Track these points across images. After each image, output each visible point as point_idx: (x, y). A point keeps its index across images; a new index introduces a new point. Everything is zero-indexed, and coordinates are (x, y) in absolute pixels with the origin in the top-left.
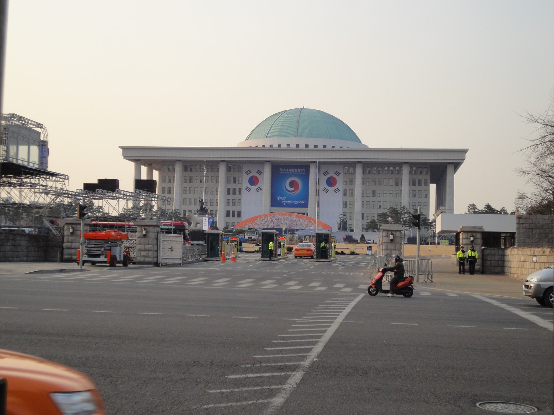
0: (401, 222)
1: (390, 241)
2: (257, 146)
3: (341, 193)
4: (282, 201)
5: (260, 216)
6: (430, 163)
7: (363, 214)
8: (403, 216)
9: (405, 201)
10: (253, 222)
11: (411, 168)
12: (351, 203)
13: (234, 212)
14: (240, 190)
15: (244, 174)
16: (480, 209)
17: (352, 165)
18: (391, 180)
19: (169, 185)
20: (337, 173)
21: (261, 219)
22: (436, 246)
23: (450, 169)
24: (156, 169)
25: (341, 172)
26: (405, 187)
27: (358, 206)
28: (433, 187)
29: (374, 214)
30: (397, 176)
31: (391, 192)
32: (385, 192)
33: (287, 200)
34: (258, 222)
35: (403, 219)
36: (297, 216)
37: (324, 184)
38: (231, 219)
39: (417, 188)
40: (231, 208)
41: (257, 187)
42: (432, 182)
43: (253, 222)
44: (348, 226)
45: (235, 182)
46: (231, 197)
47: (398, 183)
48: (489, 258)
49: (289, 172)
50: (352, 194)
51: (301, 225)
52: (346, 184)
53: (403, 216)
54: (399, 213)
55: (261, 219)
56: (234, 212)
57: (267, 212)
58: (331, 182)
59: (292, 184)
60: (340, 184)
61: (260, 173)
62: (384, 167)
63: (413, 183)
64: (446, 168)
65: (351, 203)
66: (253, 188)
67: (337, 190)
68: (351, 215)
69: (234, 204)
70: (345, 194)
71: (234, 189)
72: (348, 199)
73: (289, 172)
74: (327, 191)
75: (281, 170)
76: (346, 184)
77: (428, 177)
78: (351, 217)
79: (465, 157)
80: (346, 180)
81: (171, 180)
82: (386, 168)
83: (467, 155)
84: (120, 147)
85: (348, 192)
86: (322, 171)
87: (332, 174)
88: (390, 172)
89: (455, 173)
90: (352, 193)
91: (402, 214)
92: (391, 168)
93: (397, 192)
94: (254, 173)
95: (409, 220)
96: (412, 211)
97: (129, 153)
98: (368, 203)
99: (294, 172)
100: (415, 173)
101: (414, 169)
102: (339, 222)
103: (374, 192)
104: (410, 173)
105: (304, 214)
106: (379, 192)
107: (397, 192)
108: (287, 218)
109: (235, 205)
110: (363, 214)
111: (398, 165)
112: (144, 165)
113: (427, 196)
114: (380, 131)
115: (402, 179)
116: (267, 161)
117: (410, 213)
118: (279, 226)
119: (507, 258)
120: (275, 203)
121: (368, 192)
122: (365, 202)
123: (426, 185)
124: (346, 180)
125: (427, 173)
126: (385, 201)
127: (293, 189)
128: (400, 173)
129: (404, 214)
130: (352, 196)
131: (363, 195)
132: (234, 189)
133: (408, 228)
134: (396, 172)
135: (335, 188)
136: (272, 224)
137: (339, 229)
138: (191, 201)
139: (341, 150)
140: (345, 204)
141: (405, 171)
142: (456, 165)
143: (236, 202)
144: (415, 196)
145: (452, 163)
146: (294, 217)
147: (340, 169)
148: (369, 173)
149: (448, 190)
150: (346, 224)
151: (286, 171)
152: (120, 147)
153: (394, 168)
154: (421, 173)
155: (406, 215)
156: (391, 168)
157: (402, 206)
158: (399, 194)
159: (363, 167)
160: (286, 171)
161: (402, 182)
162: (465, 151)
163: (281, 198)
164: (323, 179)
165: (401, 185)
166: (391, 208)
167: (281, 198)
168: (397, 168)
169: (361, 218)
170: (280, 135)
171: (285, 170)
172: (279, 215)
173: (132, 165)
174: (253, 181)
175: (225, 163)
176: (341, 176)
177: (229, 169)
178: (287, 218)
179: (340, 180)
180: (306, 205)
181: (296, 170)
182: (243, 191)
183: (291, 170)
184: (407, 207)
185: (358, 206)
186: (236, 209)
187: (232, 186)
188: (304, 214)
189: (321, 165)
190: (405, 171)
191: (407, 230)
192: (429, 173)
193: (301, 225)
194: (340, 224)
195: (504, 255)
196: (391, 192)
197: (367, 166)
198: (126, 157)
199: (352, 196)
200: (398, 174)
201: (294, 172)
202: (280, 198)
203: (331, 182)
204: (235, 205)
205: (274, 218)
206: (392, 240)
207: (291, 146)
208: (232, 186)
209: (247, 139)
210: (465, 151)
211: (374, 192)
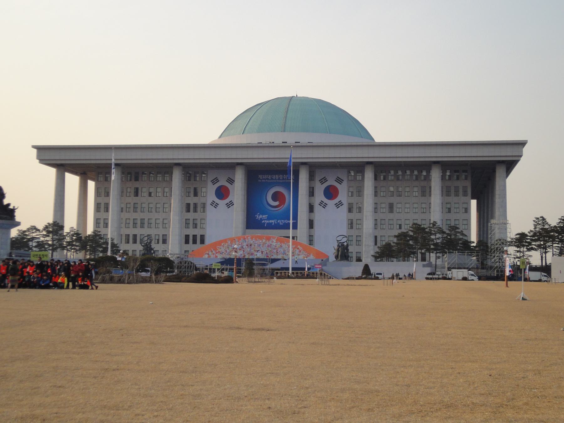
0: (430, 245)
3: (345, 208)
4: (261, 219)
5: (225, 241)
7: (376, 237)
8: (433, 237)
9: (436, 215)
10: (215, 250)
11: (444, 172)
12: (359, 222)
13: (195, 237)
14: (204, 206)
15: (210, 184)
16: (553, 225)
17: (358, 168)
18: (416, 189)
19: (105, 200)
20: (339, 181)
21: (226, 245)
22: (504, 283)
23: (500, 171)
24: (92, 179)
25: (344, 176)
26: (436, 198)
27: (368, 225)
28: (474, 203)
29: (390, 236)
30: (423, 184)
31: (416, 206)
32: (407, 206)
33: (268, 219)
34: (222, 250)
35: (433, 240)
37: (319, 196)
38: (191, 247)
40: (191, 232)
41: (227, 201)
43: (215, 250)
45: (196, 194)
46: (191, 215)
47: (426, 192)
49: (272, 179)
50: (360, 210)
53: (433, 237)
54: (426, 233)
55: (226, 245)
56: (195, 237)
57: (240, 234)
58: (331, 193)
60: (343, 196)
61: (231, 181)
62: (403, 169)
64: (494, 171)
65: (359, 222)
66: (222, 203)
68: (359, 239)
69: (195, 226)
70: (350, 210)
71: (195, 205)
72: (354, 216)
73: (272, 179)
74: (325, 206)
75: (260, 176)
78: (359, 242)
79: (522, 151)
80: (351, 189)
81: (107, 194)
82: (408, 172)
83: (525, 149)
84: (34, 147)
85: (355, 207)
86: (318, 178)
87: (331, 182)
88: (414, 177)
89: (507, 176)
90: (360, 208)
91: (431, 234)
92: (416, 173)
93: (424, 206)
94: (223, 182)
95: (442, 243)
97: (49, 155)
98: (383, 222)
99: (279, 179)
102: (336, 247)
103: (391, 207)
104: (443, 178)
106: (399, 206)
107: (424, 206)
108: (264, 244)
109: (196, 227)
110: (376, 237)
111: (425, 166)
113: (467, 210)
114: (395, 119)
115: (430, 187)
117: (444, 233)
118: (252, 254)
120: (252, 223)
121: (383, 206)
122: (379, 221)
124: (351, 189)
125: (466, 179)
126: (406, 217)
127: (277, 203)
128: (428, 178)
129: (435, 234)
130: (360, 212)
131: (376, 210)
132: (195, 205)
133: (440, 255)
134: (422, 178)
135: (336, 201)
136: (242, 252)
137: (337, 257)
140: (351, 225)
141: (369, 175)
142: (510, 165)
143: (198, 222)
147: (342, 174)
148: (384, 179)
149: (497, 200)
151: (268, 179)
152: (34, 147)
153: (420, 172)
154: (458, 178)
155: (438, 235)
157: (432, 222)
160: (268, 179)
161: (430, 191)
162: (523, 144)
163: (261, 216)
164: (320, 189)
165: (430, 196)
166: (414, 224)
167: (261, 216)
169: (373, 243)
171: (266, 177)
172: (252, 238)
173: (53, 171)
174: (222, 193)
175: (181, 167)
176: (345, 183)
178: (264, 244)
179: (343, 189)
181: (281, 176)
182: (209, 207)
183: (274, 177)
184: (439, 223)
185: (368, 225)
186: (198, 232)
187: (192, 200)
189: (314, 168)
190: (369, 175)
191: (439, 257)
192: (469, 178)
194: (338, 250)
196: (416, 206)
197: (383, 169)
198: (43, 161)
199: (360, 212)
200: (425, 180)
201: (279, 179)
202: (259, 217)
203: (331, 193)
204: (196, 227)
205: (245, 244)
208: (192, 200)
209: (220, 137)
210: (523, 144)
211: (391, 207)
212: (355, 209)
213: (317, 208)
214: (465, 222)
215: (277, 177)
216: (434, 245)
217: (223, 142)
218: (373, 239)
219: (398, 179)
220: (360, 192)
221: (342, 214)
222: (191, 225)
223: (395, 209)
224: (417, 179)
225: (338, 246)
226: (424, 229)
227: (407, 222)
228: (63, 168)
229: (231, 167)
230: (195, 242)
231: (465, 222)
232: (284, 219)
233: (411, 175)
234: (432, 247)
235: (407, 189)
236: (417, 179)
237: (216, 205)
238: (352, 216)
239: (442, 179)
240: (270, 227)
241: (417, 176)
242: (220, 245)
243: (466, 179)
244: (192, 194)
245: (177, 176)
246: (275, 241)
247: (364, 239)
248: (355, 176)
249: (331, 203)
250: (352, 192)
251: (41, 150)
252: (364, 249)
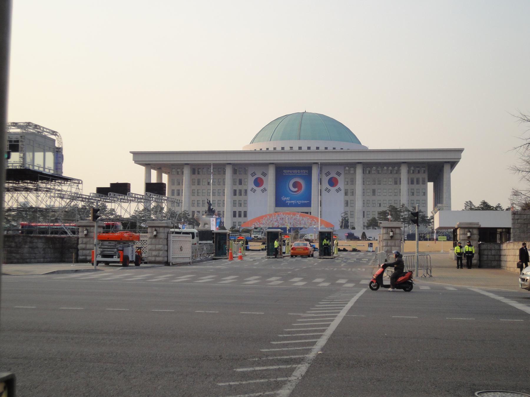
1: (390, 238)
2: (261, 149)
3: (343, 192)
5: (266, 216)
6: (428, 163)
7: (364, 212)
8: (402, 214)
10: (259, 222)
16: (477, 206)
17: (353, 165)
18: (390, 180)
19: (178, 187)
20: (339, 174)
21: (266, 219)
23: (446, 168)
24: (165, 173)
25: (341, 171)
26: (404, 186)
27: (359, 205)
29: (374, 212)
32: (385, 191)
33: (290, 200)
34: (264, 222)
35: (402, 216)
36: (300, 216)
37: (325, 185)
38: (237, 219)
39: (415, 186)
40: (237, 209)
41: (262, 188)
42: (429, 181)
43: (259, 222)
44: (349, 224)
45: (240, 183)
46: (237, 198)
47: (397, 182)
48: (486, 252)
50: (353, 193)
51: (305, 224)
52: (347, 184)
53: (402, 214)
55: (266, 219)
57: (272, 212)
58: (333, 182)
59: (295, 185)
60: (341, 184)
61: (264, 174)
63: (411, 182)
64: (443, 167)
67: (338, 190)
68: (352, 213)
69: (240, 205)
70: (346, 194)
73: (293, 173)
75: (285, 171)
76: (347, 184)
77: (426, 176)
78: (352, 215)
79: (461, 156)
80: (347, 180)
81: (180, 183)
82: (385, 168)
83: (463, 154)
84: (131, 152)
85: (349, 191)
86: (324, 171)
87: (333, 175)
88: (389, 171)
89: (451, 172)
90: (353, 192)
92: (390, 168)
93: (396, 191)
94: (259, 175)
95: (408, 218)
96: (411, 209)
98: (368, 202)
99: (298, 173)
100: (413, 173)
101: (412, 168)
102: (341, 220)
103: (374, 191)
104: (409, 172)
105: (307, 213)
106: (379, 191)
107: (396, 191)
109: (241, 206)
110: (364, 212)
112: (154, 169)
113: (425, 194)
114: (379, 132)
115: (400, 179)
116: (358, 163)
117: (409, 211)
118: (284, 225)
119: (503, 253)
120: (279, 203)
121: (368, 191)
123: (424, 183)
124: (347, 180)
125: (424, 172)
126: (384, 200)
127: (296, 189)
128: (398, 172)
130: (353, 195)
133: (407, 225)
134: (395, 172)
135: (337, 187)
137: (341, 227)
138: (199, 191)
139: (342, 151)
140: (347, 203)
141: (404, 170)
142: (453, 164)
144: (413, 195)
145: (448, 162)
146: (298, 217)
150: (348, 222)
151: (290, 173)
152: (131, 152)
153: (393, 167)
154: (419, 172)
155: (406, 213)
156: (390, 168)
158: (398, 193)
159: (363, 168)
160: (290, 173)
161: (400, 182)
162: (461, 151)
163: (285, 198)
164: (325, 180)
165: (400, 184)
167: (285, 198)
168: (396, 168)
169: (362, 216)
170: (282, 139)
171: (288, 171)
172: (283, 214)
173: (143, 168)
174: (258, 182)
175: (231, 166)
176: (342, 176)
177: (235, 172)
180: (309, 205)
181: (299, 171)
182: (249, 192)
183: (294, 171)
185: (359, 205)
186: (242, 209)
187: (238, 187)
188: (307, 213)
189: (322, 166)
190: (404, 170)
191: (406, 227)
192: (427, 173)
193: (305, 224)
194: (342, 222)
195: (500, 250)
196: (390, 191)
197: (367, 166)
198: (136, 162)
199: (353, 195)
200: (396, 173)
202: (284, 199)
203: (333, 182)
204: (241, 206)
205: (279, 218)
206: (392, 237)
207: (293, 149)
208: (238, 187)
209: (252, 142)
210: (461, 151)
211: (374, 191)
212: (349, 194)
213: (324, 192)
214: (423, 202)
215: (296, 171)
216: (403, 219)
217: (252, 148)
218: (362, 214)
219: (379, 173)
220: (353, 181)
221: (341, 197)
222: (237, 205)
223: (376, 193)
224: (391, 173)
225: (342, 219)
226: (189, 224)
227: (385, 202)
228: (149, 166)
229: (266, 165)
230: (240, 216)
231: (423, 202)
232: (301, 200)
233: (387, 169)
234: (402, 220)
235: (385, 180)
236: (391, 173)
237: (254, 191)
238: (347, 198)
239: (408, 173)
240: (291, 205)
241: (413, 171)
242: (262, 219)
243: (424, 172)
244: (196, 183)
245: (187, 171)
246: (298, 216)
247: (356, 214)
248: (349, 170)
249: (333, 189)
250: (347, 182)
251: (135, 154)
252: (356, 220)
